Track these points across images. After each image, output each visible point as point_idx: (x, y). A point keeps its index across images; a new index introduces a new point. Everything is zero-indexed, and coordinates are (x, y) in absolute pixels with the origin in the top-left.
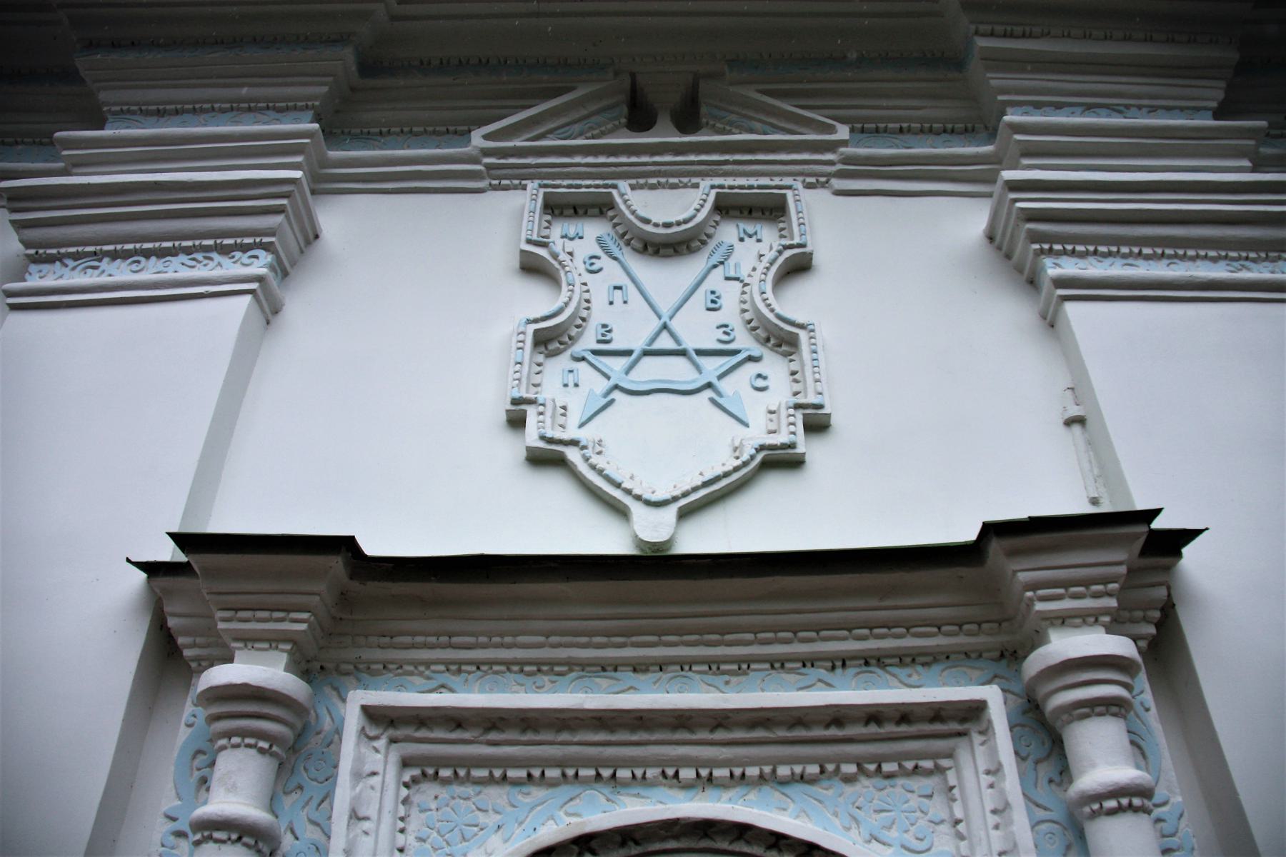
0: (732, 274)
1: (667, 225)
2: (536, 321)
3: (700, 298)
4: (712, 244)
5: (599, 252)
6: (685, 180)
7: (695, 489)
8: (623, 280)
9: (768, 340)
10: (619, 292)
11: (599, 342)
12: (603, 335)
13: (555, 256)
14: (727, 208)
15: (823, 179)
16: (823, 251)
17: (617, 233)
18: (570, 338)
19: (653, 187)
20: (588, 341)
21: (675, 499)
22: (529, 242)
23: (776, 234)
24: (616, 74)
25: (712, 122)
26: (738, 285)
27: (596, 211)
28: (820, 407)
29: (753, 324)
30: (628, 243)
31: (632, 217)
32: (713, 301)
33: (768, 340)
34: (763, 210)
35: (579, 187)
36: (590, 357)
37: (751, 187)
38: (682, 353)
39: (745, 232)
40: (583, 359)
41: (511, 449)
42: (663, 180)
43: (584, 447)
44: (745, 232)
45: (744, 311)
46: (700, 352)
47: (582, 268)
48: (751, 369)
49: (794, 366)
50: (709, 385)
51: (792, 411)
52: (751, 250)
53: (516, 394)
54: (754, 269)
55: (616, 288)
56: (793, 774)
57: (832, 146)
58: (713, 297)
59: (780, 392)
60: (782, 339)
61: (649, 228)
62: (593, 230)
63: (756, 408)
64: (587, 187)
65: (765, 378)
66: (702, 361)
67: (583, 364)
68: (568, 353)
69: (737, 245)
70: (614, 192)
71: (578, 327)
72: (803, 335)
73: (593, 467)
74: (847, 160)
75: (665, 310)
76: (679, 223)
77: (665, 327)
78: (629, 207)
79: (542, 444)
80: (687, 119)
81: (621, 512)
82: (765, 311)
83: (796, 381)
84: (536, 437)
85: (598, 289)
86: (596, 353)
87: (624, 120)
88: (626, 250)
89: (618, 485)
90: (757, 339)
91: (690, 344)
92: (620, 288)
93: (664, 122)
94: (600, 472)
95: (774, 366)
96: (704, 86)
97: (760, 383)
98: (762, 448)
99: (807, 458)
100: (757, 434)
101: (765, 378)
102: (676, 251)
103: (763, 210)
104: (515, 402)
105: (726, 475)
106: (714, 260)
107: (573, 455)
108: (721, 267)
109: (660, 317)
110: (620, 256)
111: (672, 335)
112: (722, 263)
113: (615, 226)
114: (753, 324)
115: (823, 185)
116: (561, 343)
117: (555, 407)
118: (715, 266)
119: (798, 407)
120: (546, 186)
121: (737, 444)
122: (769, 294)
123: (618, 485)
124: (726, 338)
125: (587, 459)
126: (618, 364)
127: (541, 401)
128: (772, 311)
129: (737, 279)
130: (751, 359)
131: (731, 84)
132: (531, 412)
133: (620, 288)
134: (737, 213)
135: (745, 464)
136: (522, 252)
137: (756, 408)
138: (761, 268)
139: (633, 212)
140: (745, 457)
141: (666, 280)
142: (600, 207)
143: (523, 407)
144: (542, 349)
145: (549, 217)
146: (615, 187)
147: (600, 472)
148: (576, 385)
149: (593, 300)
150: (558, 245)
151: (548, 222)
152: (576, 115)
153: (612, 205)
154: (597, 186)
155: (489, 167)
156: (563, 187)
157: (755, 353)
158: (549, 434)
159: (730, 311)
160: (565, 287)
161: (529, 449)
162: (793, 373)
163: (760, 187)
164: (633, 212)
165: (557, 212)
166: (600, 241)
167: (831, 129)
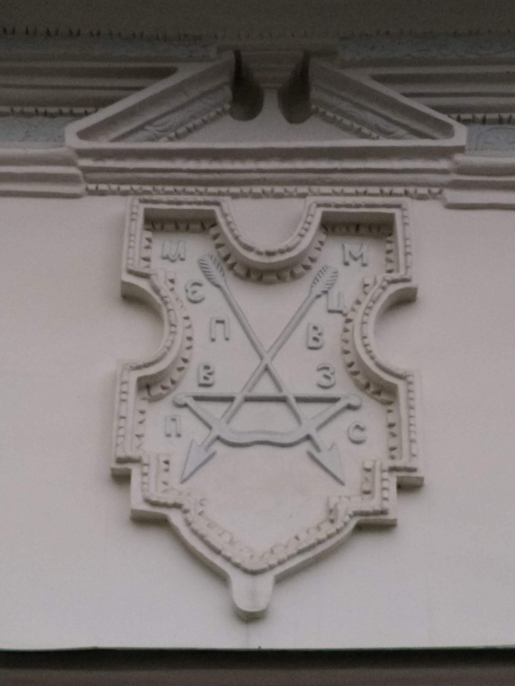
0: (334, 306)
1: (270, 254)
2: (139, 368)
3: (300, 335)
4: (316, 268)
5: (200, 277)
6: (291, 189)
7: (290, 557)
8: (226, 313)
9: (367, 386)
10: (219, 326)
11: (202, 385)
12: (206, 378)
13: (157, 291)
14: (334, 226)
15: (435, 190)
16: (427, 275)
17: (219, 254)
18: (173, 382)
19: (257, 196)
20: (189, 386)
21: (271, 567)
22: (131, 272)
23: (382, 256)
24: (220, 50)
25: (321, 110)
26: (340, 318)
27: (198, 227)
28: (413, 470)
29: (354, 369)
30: (231, 267)
31: (234, 243)
32: (315, 339)
33: (367, 386)
34: (370, 227)
35: (179, 203)
36: (192, 403)
37: (358, 206)
38: (283, 400)
39: (350, 254)
40: (186, 405)
41: (108, 508)
42: (268, 189)
43: (186, 511)
44: (350, 254)
45: (346, 352)
46: (300, 400)
47: (183, 296)
48: (349, 419)
49: (391, 418)
50: (308, 438)
51: (386, 475)
52: (351, 271)
53: (121, 454)
54: (358, 302)
55: (218, 322)
56: (352, 126)
57: (446, 153)
58: (315, 334)
59: (375, 451)
60: (381, 388)
61: (252, 256)
62: (195, 248)
63: (350, 462)
64: (190, 201)
65: (362, 429)
66: (304, 409)
67: (185, 412)
68: (168, 400)
69: (342, 270)
70: (216, 209)
71: (180, 369)
72: (401, 385)
73: (195, 532)
74: (462, 170)
75: (266, 343)
76: (282, 252)
77: (267, 369)
78: (232, 231)
79: (146, 508)
80: (297, 102)
81: (221, 577)
82: (366, 358)
83: (394, 435)
84: (140, 499)
85: (201, 318)
86: (198, 398)
87: (227, 107)
88: (229, 275)
89: (218, 552)
90: (357, 384)
91: (291, 391)
92: (222, 322)
93: (271, 109)
94: (202, 538)
95: (371, 415)
96: (317, 65)
97: (357, 435)
98: (356, 514)
99: (399, 522)
100: (352, 503)
101: (362, 429)
102: (279, 277)
103: (370, 227)
104: (120, 461)
105: (320, 542)
106: (318, 289)
107: (176, 518)
108: (324, 297)
109: (261, 358)
110: (222, 284)
111: (274, 379)
112: (326, 292)
113: (218, 246)
114: (354, 369)
115: (434, 196)
116: (164, 388)
117: (158, 461)
118: (318, 296)
119: (393, 469)
120: (146, 201)
121: (332, 506)
122: (369, 330)
123: (218, 552)
124: (325, 382)
125: (189, 524)
126: (216, 410)
127: (145, 460)
128: (372, 358)
129: (340, 312)
130: (350, 407)
131: (345, 65)
132: (135, 471)
133: (222, 322)
134: (344, 230)
135: (338, 531)
136: (124, 284)
137: (350, 462)
138: (366, 301)
139: (236, 238)
140: (339, 525)
141: (268, 308)
142: (203, 224)
143: (129, 466)
144: (145, 394)
145: (149, 234)
146: (218, 204)
147: (202, 538)
148: (179, 435)
149: (196, 338)
150: (160, 269)
151: (149, 240)
152: (176, 103)
153: (214, 224)
154: (199, 203)
155: (86, 170)
156: (165, 201)
157: (354, 402)
158: (154, 499)
159: (331, 352)
160: (167, 328)
161: (133, 511)
162: (391, 425)
163: (368, 206)
164: (236, 238)
165: (158, 226)
166: (203, 266)
167: (447, 130)
